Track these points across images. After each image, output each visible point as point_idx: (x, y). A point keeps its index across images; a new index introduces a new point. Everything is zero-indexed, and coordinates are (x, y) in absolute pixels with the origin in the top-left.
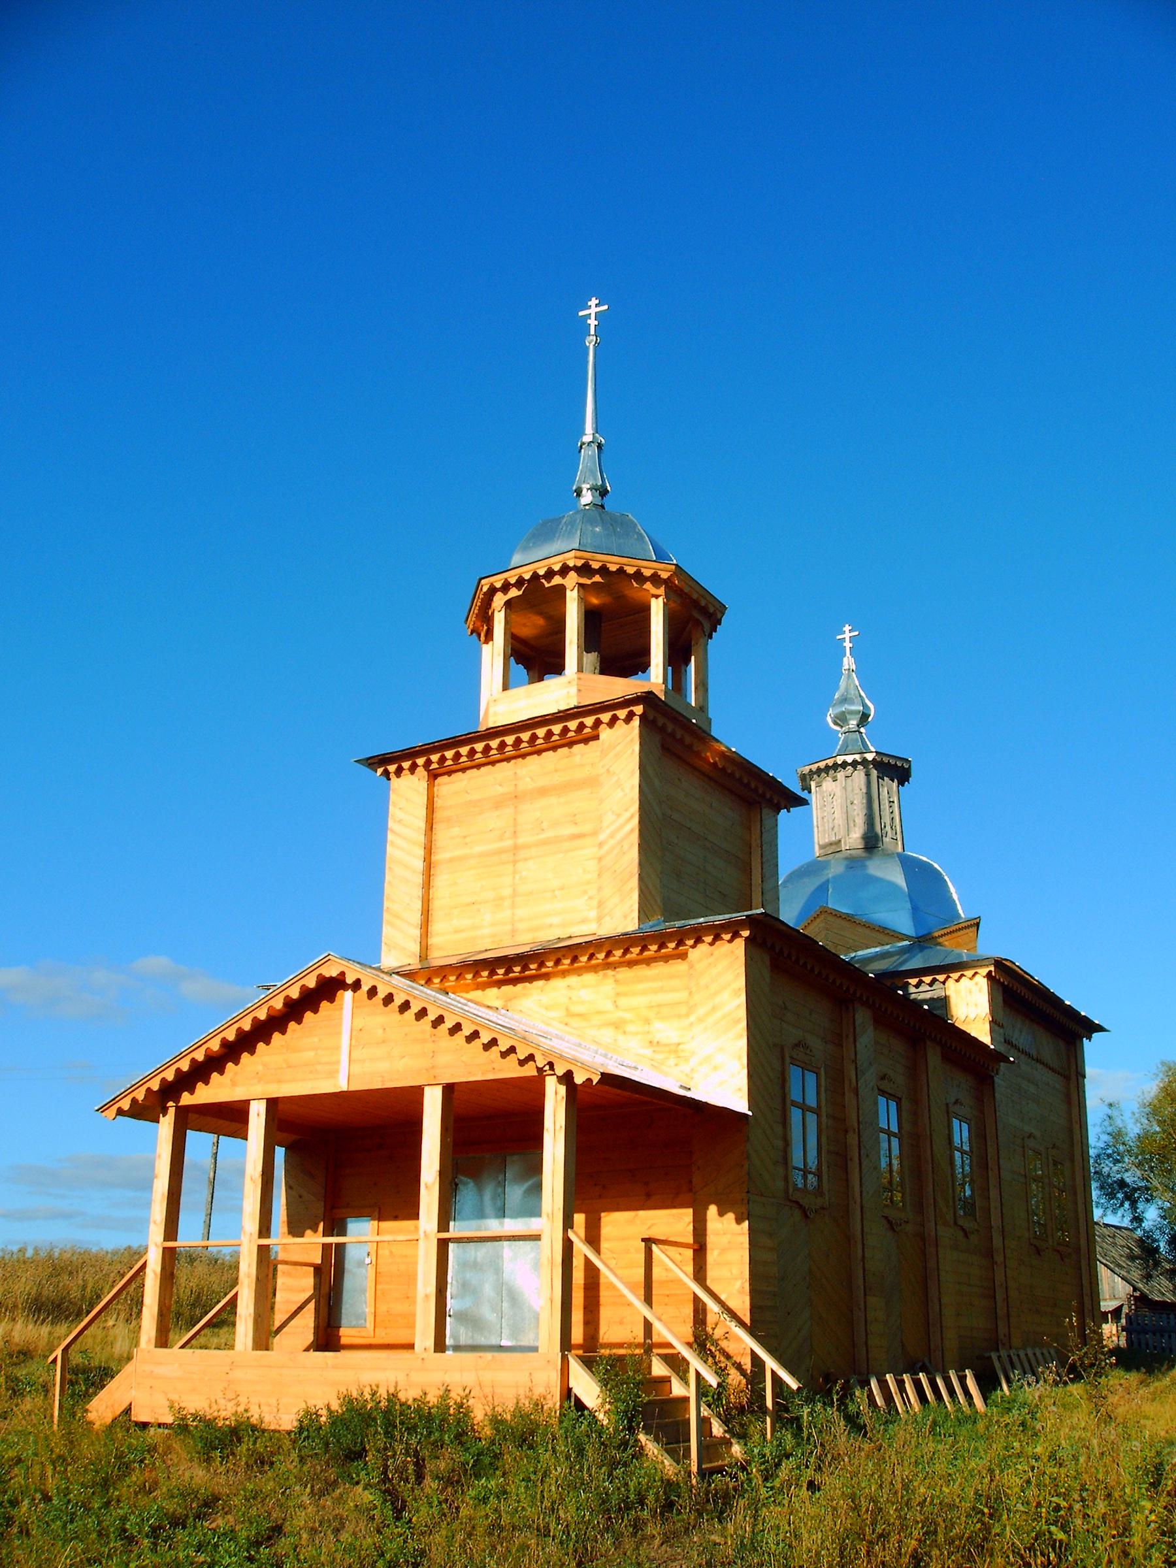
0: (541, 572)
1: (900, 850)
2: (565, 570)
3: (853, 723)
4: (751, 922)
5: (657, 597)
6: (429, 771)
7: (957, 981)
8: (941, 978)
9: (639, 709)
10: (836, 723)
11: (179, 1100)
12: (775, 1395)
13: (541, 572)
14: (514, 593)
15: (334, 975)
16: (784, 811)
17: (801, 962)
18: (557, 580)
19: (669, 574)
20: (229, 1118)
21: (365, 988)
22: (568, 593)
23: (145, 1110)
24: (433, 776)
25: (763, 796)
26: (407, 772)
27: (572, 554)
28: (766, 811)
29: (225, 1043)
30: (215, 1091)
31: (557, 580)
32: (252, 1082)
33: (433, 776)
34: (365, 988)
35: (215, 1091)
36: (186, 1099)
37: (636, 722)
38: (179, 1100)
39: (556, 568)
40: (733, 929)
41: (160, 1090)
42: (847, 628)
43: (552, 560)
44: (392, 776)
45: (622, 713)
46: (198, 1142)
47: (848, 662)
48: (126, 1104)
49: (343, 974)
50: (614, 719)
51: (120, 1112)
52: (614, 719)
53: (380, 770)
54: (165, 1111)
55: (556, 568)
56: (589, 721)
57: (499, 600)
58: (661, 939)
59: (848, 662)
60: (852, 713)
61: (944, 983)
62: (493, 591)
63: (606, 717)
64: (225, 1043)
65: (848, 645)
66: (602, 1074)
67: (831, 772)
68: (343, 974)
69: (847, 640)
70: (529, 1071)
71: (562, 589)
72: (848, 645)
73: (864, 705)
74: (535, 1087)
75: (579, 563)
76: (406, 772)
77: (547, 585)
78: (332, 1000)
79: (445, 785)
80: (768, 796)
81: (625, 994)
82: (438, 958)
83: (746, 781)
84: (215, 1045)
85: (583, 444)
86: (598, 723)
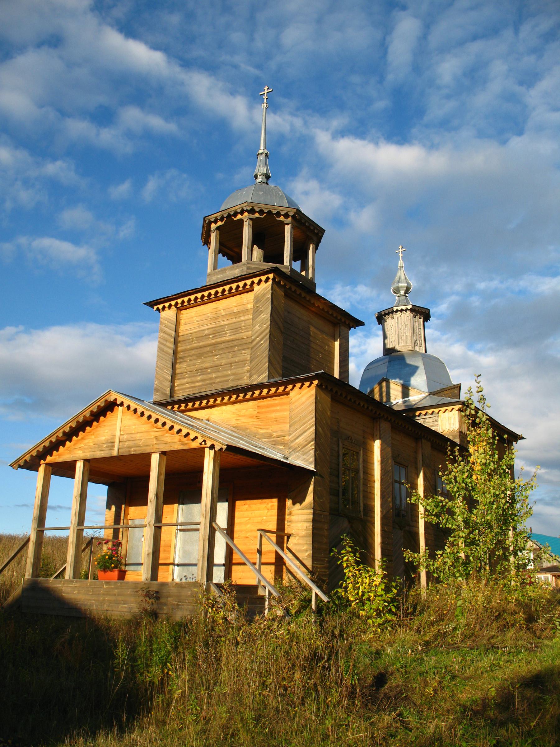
0: (232, 213)
1: (424, 352)
2: (242, 213)
3: (402, 292)
4: (317, 377)
5: (288, 224)
6: (177, 308)
7: (444, 412)
8: (436, 410)
9: (271, 276)
10: (395, 293)
11: (44, 459)
12: (35, 565)
13: (232, 213)
14: (220, 223)
15: (112, 400)
16: (352, 329)
17: (348, 398)
18: (239, 217)
19: (293, 213)
20: (66, 469)
21: (125, 405)
22: (244, 223)
23: (31, 464)
24: (179, 309)
25: (341, 320)
26: (167, 309)
27: (246, 204)
28: (342, 328)
29: (64, 433)
30: (62, 455)
31: (239, 217)
32: (78, 451)
33: (179, 309)
34: (125, 405)
35: (62, 455)
36: (49, 459)
37: (270, 282)
38: (44, 459)
39: (239, 211)
40: (310, 379)
41: (36, 456)
42: (400, 247)
43: (237, 208)
44: (161, 310)
45: (264, 278)
46: (55, 480)
47: (401, 263)
48: (22, 463)
49: (116, 399)
50: (260, 281)
51: (20, 467)
52: (260, 281)
53: (156, 307)
54: (40, 465)
55: (239, 211)
56: (249, 282)
57: (213, 226)
58: (277, 385)
59: (401, 263)
60: (402, 287)
61: (438, 413)
62: (210, 223)
63: (256, 280)
64: (64, 433)
65: (401, 255)
66: (227, 445)
67: (391, 315)
68: (116, 399)
69: (401, 252)
70: (195, 445)
71: (241, 221)
72: (401, 255)
73: (408, 283)
74: (200, 452)
75: (249, 208)
76: (167, 309)
77: (235, 219)
78: (112, 411)
79: (185, 314)
80: (343, 320)
81: (262, 413)
82: (180, 395)
83: (330, 313)
84: (60, 434)
85: (259, 154)
86: (253, 283)
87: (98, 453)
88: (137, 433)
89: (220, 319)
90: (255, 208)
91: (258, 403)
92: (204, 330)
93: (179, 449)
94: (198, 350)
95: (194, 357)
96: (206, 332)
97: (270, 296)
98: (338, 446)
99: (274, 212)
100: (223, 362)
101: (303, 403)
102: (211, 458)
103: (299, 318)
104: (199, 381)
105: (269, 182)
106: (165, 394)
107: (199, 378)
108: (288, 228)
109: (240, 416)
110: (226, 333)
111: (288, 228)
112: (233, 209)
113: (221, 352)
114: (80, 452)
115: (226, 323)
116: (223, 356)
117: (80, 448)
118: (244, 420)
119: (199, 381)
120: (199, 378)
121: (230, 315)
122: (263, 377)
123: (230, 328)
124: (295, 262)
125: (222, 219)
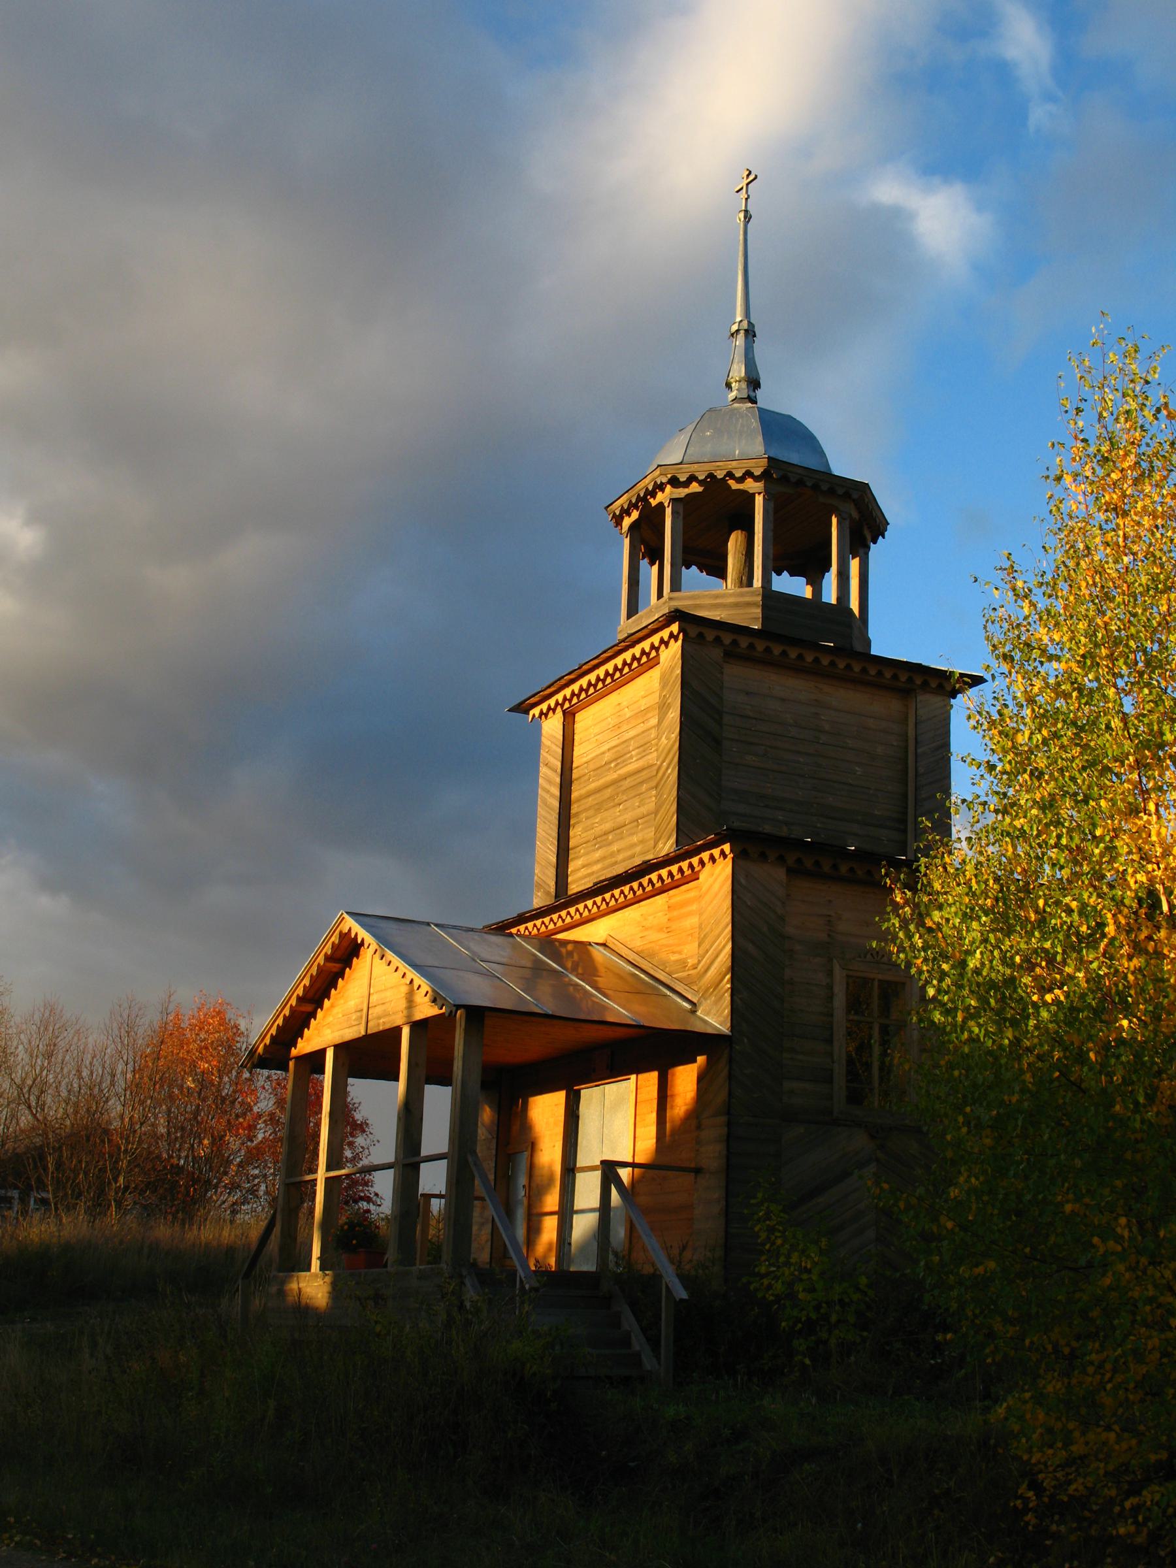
9: (675, 628)
49: (350, 930)
87: (347, 1031)
88: (385, 990)
89: (625, 727)
90: (678, 476)
91: (670, 898)
92: (603, 753)
93: (429, 1015)
94: (598, 795)
95: (591, 812)
96: (607, 757)
97: (679, 671)
98: (830, 973)
99: (720, 475)
100: (628, 817)
101: (716, 895)
102: (341, 1033)
103: (783, 700)
104: (598, 861)
105: (759, 394)
106: (548, 893)
107: (598, 855)
108: (759, 501)
109: (647, 929)
110: (631, 757)
111: (759, 501)
112: (642, 484)
113: (625, 798)
114: (328, 1031)
115: (632, 733)
116: (628, 804)
117: (329, 1025)
118: (654, 936)
119: (598, 861)
120: (598, 855)
121: (636, 716)
122: (667, 846)
123: (637, 745)
124: (779, 574)
125: (636, 506)
